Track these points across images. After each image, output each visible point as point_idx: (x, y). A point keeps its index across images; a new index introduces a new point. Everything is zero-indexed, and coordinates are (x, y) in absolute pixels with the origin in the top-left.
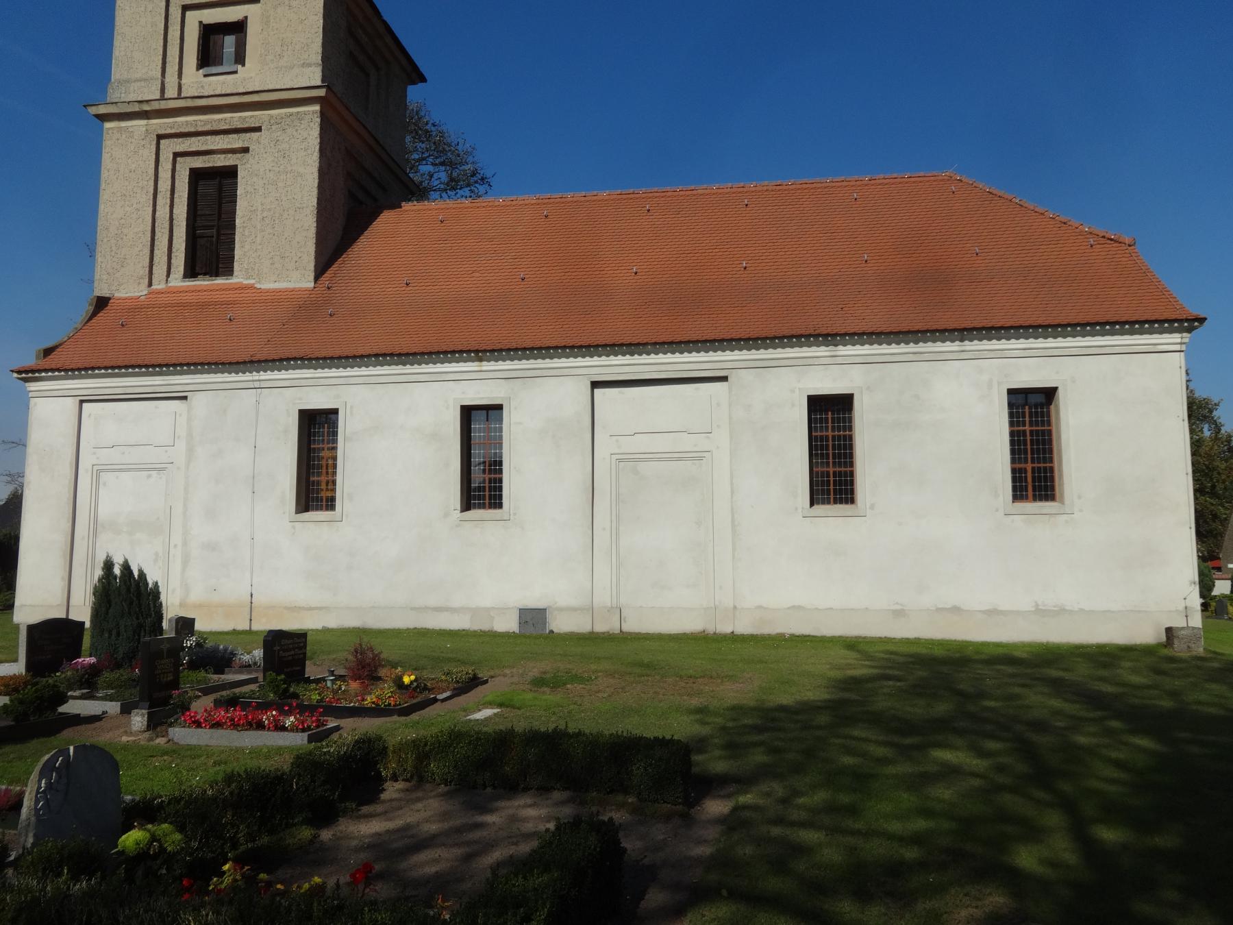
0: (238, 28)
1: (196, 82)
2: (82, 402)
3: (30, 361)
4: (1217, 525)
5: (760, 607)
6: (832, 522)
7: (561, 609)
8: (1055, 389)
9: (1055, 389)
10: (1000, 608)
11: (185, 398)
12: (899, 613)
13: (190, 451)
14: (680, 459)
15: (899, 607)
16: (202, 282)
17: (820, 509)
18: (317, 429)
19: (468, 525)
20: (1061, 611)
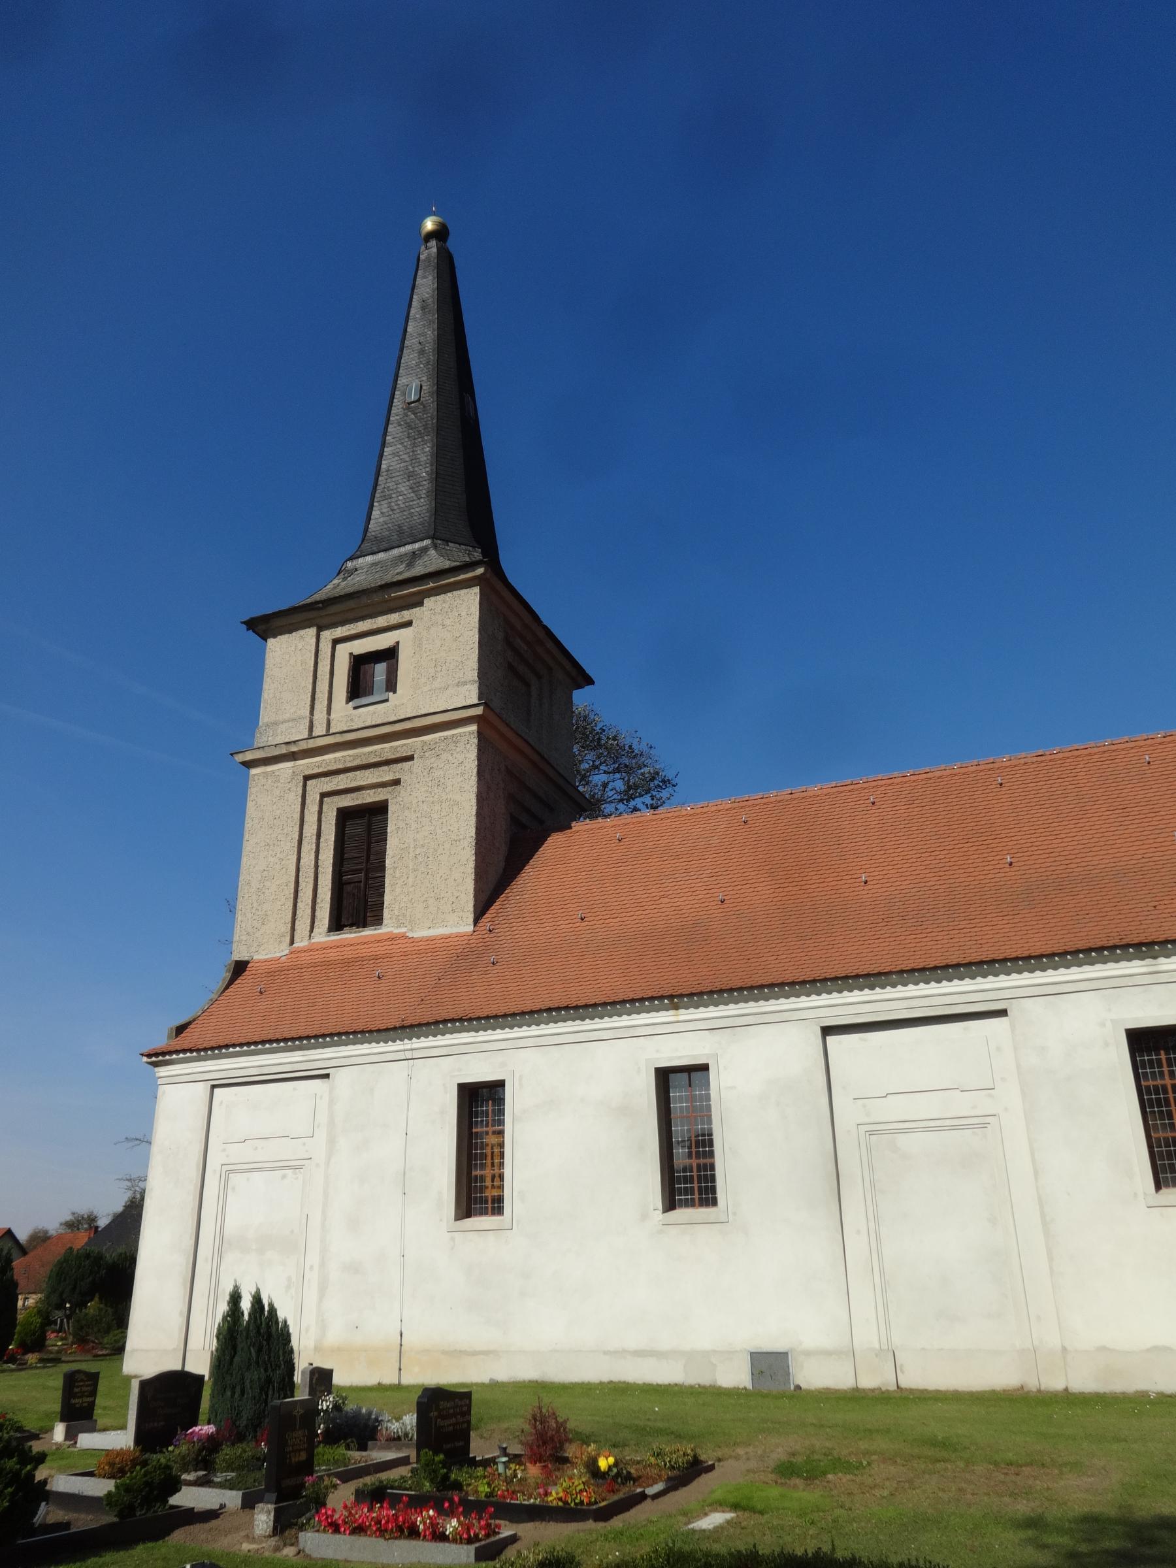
0: (390, 655)
1: (347, 716)
3: (161, 1040)
7: (808, 1353)
8: (501, 1084)
11: (327, 1076)
13: (332, 1141)
16: (349, 935)
18: (480, 1104)
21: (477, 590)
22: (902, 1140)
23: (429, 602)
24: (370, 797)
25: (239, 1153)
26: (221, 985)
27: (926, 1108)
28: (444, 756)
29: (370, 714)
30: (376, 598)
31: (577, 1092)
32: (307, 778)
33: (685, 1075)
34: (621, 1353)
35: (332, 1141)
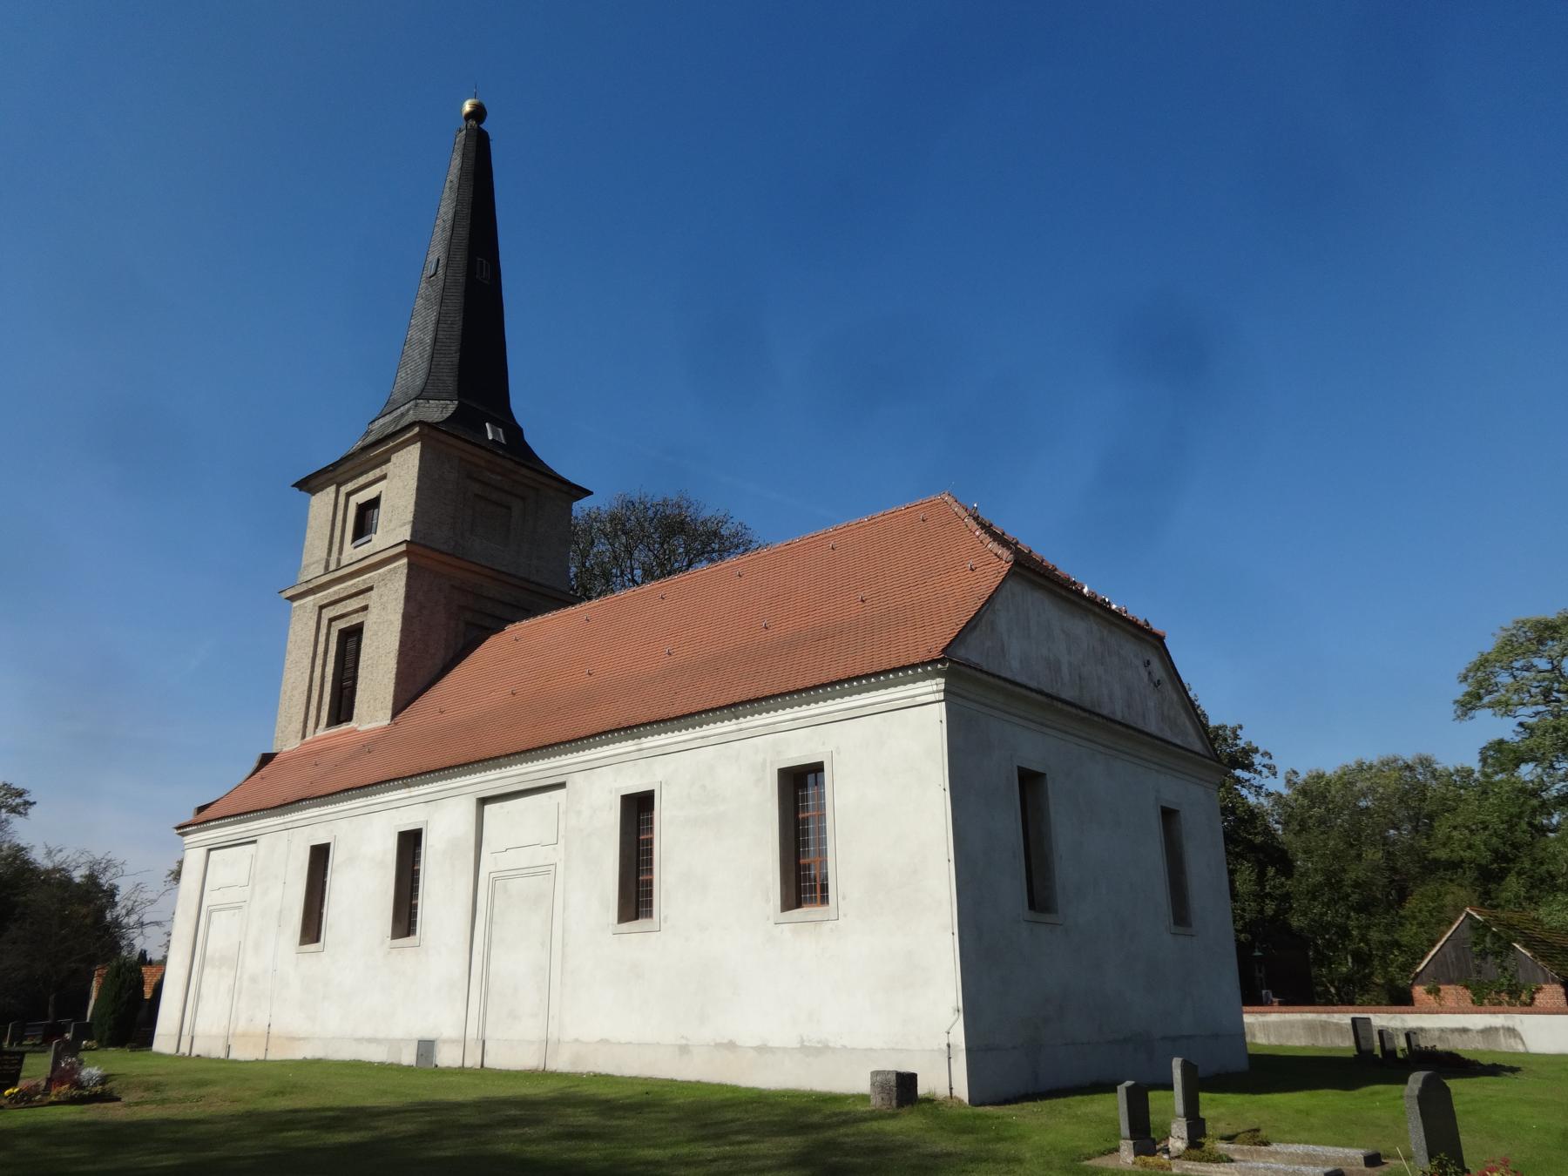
0: (375, 503)
1: (351, 553)
3: (189, 817)
5: (577, 1040)
7: (445, 1041)
10: (771, 1044)
12: (684, 1049)
14: (534, 874)
15: (684, 1042)
16: (334, 730)
17: (626, 926)
18: (799, 787)
20: (822, 1050)
21: (419, 445)
23: (394, 458)
26: (250, 771)
27: (521, 859)
29: (365, 550)
30: (364, 457)
32: (321, 608)
34: (359, 1040)
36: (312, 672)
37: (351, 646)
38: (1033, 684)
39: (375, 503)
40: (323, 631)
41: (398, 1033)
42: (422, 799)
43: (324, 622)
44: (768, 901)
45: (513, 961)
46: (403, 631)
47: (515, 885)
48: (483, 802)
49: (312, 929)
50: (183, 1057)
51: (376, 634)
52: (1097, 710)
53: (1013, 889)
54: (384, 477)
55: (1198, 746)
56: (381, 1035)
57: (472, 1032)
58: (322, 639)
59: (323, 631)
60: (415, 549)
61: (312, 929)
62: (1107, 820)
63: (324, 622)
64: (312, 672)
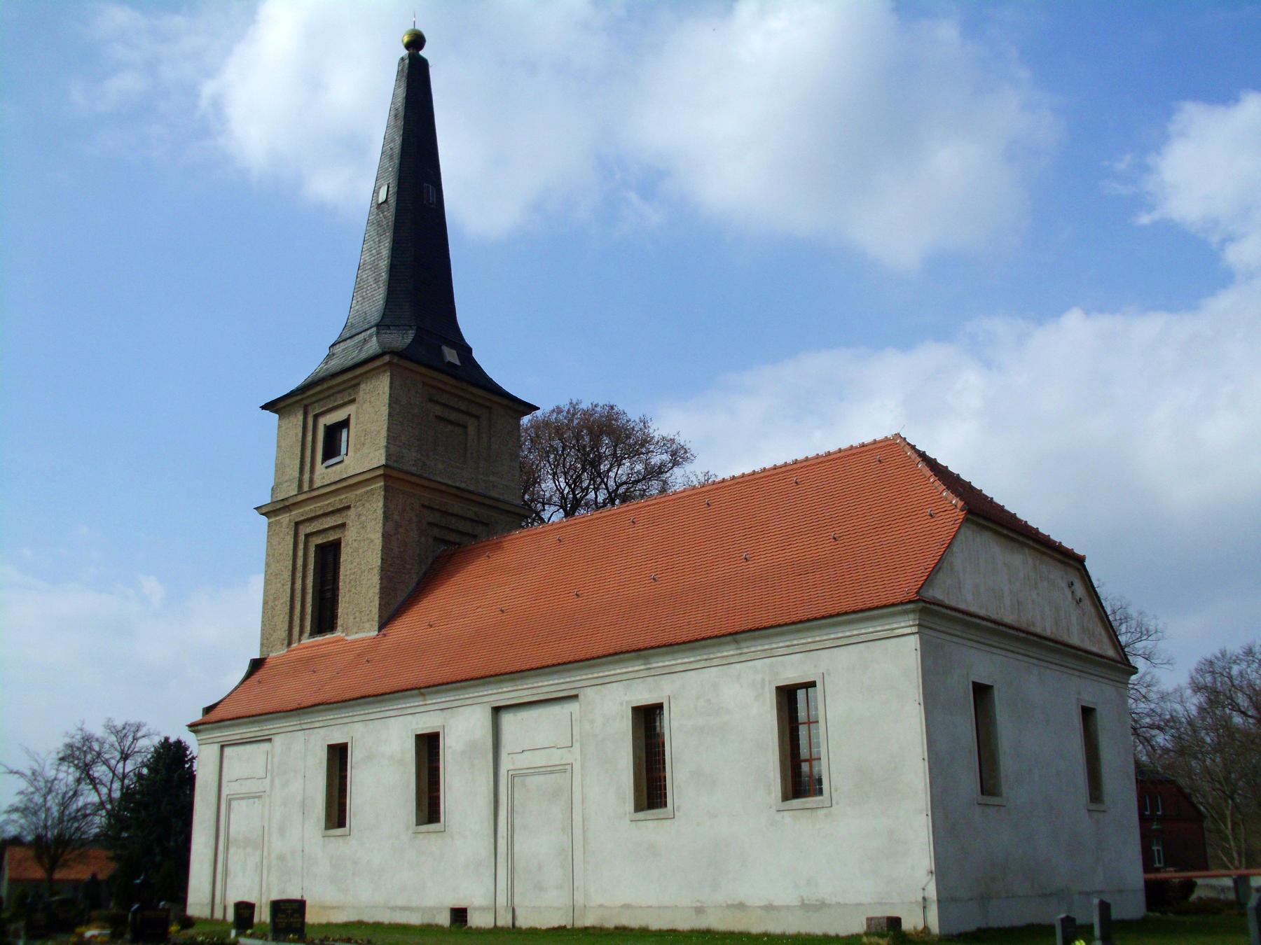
0: (345, 424)
1: (324, 474)
2: (222, 747)
4: (263, 915)
5: (601, 906)
6: (652, 827)
7: (475, 909)
8: (660, 706)
9: (660, 706)
10: (775, 904)
11: (575, 697)
12: (700, 910)
13: (272, 781)
14: (552, 772)
15: (699, 904)
16: (319, 639)
17: (641, 815)
18: (338, 756)
19: (420, 836)
20: (821, 906)
22: (529, 779)
24: (332, 537)
25: (523, 761)
27: (539, 759)
28: (367, 505)
31: (382, 748)
32: (297, 524)
33: (804, 691)
34: (393, 909)
35: (272, 781)
36: (293, 583)
37: (330, 559)
38: (982, 613)
39: (345, 424)
40: (301, 546)
41: (430, 901)
42: (436, 707)
43: (302, 538)
44: (770, 793)
45: (537, 844)
46: (384, 548)
47: (533, 781)
48: (497, 710)
49: (337, 814)
50: (217, 921)
51: (357, 550)
52: (1032, 629)
53: (969, 781)
54: (353, 401)
55: (1111, 653)
56: (414, 904)
57: (502, 900)
58: (300, 553)
59: (301, 546)
60: (392, 476)
61: (337, 814)
62: (1037, 716)
63: (302, 538)
64: (293, 583)
